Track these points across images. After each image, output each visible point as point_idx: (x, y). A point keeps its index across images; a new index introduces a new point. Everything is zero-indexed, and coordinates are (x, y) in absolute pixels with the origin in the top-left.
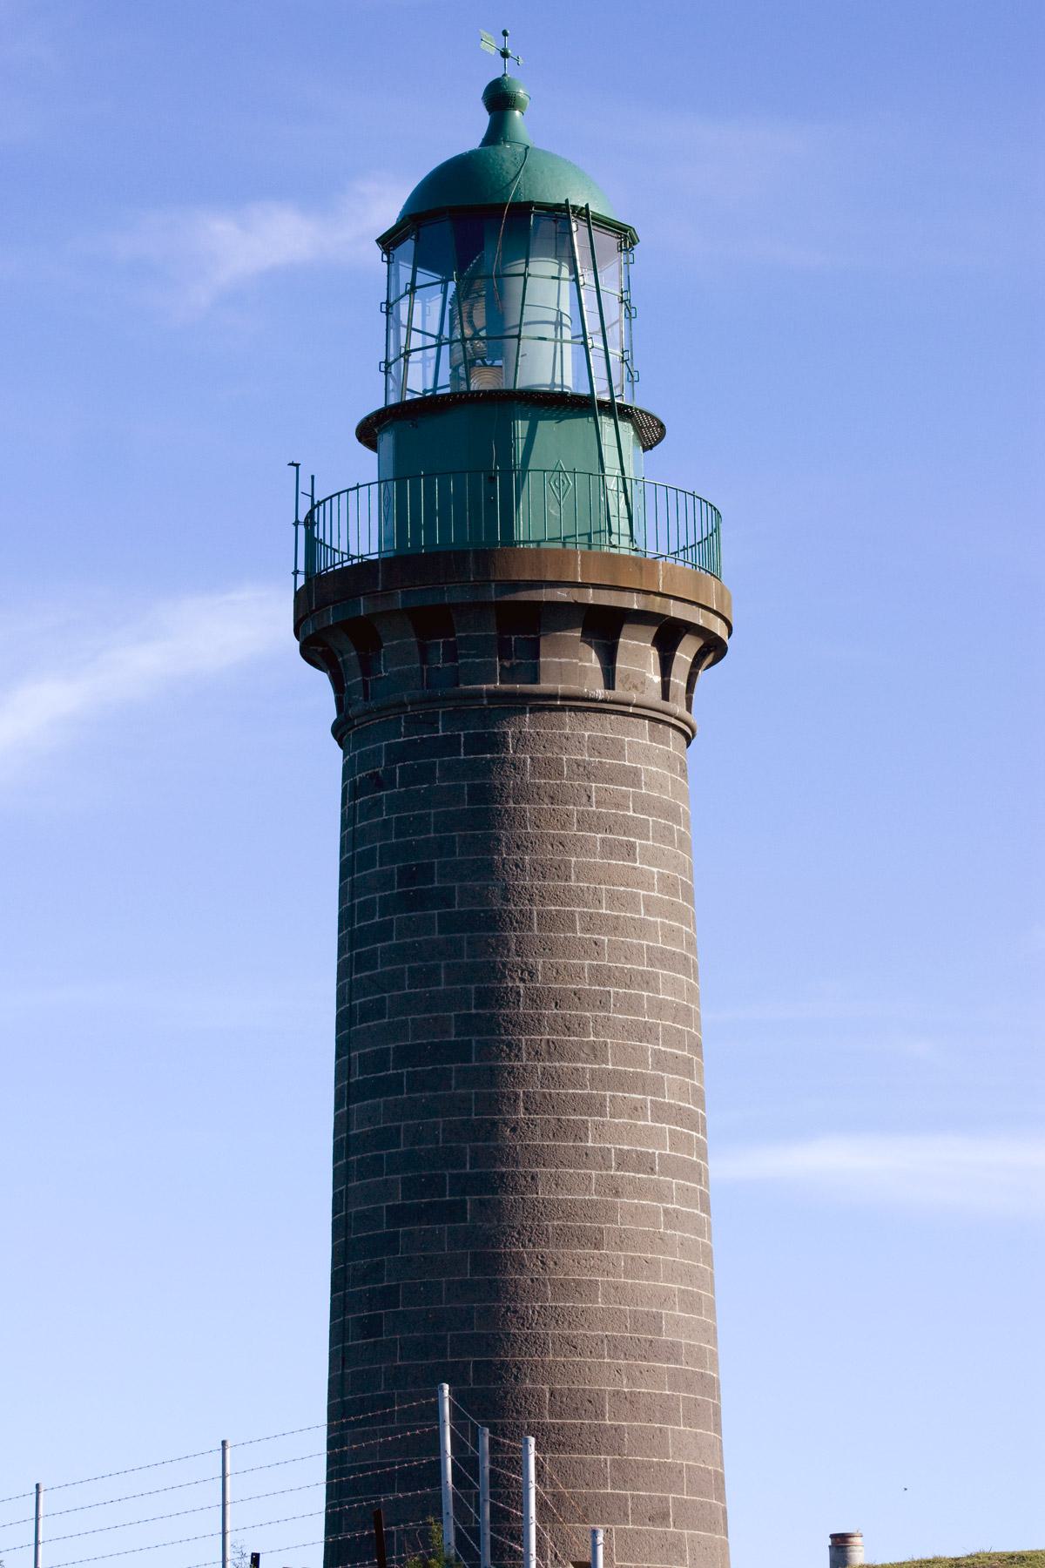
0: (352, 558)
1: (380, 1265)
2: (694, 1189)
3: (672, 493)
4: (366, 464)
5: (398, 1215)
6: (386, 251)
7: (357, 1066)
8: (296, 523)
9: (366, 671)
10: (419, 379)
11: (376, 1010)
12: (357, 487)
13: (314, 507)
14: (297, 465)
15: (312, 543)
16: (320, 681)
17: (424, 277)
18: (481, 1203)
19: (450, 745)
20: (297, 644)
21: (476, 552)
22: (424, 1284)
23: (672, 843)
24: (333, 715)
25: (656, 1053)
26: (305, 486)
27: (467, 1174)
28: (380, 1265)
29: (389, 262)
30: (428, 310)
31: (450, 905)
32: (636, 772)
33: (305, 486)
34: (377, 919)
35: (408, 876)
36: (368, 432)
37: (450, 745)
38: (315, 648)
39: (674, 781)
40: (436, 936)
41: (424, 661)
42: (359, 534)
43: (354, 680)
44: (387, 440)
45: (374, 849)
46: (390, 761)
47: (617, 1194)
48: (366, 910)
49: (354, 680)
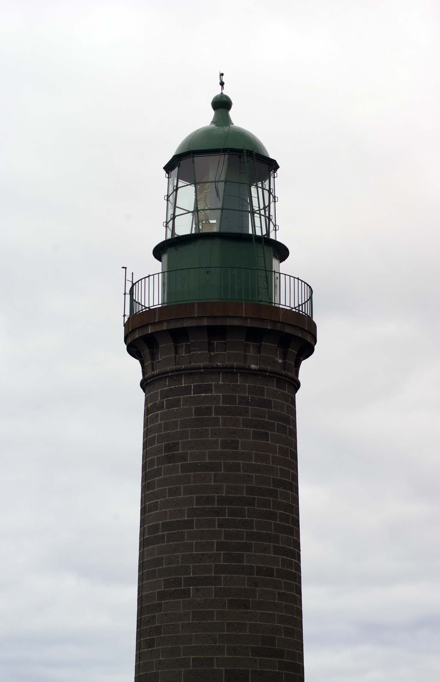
0: (146, 308)
1: (154, 616)
2: (293, 584)
3: (287, 277)
4: (157, 266)
5: (162, 595)
6: (167, 172)
7: (146, 532)
8: (125, 294)
9: (153, 359)
10: (185, 227)
11: (155, 507)
12: (145, 278)
13: (133, 285)
14: (126, 268)
15: (132, 300)
16: (136, 364)
17: (181, 184)
18: (197, 589)
19: (187, 390)
20: (126, 346)
21: (198, 304)
22: (172, 625)
23: (286, 433)
24: (141, 377)
25: (276, 525)
26: (129, 277)
27: (191, 577)
28: (154, 616)
29: (168, 178)
30: (187, 195)
31: (186, 461)
32: (270, 402)
33: (129, 277)
34: (155, 467)
35: (169, 448)
36: (159, 252)
37: (187, 390)
38: (133, 349)
39: (288, 406)
40: (180, 474)
41: (176, 353)
42: (153, 297)
43: (148, 363)
44: (165, 257)
45: (154, 437)
46: (162, 398)
47: (257, 586)
48: (152, 463)
49: (148, 363)
